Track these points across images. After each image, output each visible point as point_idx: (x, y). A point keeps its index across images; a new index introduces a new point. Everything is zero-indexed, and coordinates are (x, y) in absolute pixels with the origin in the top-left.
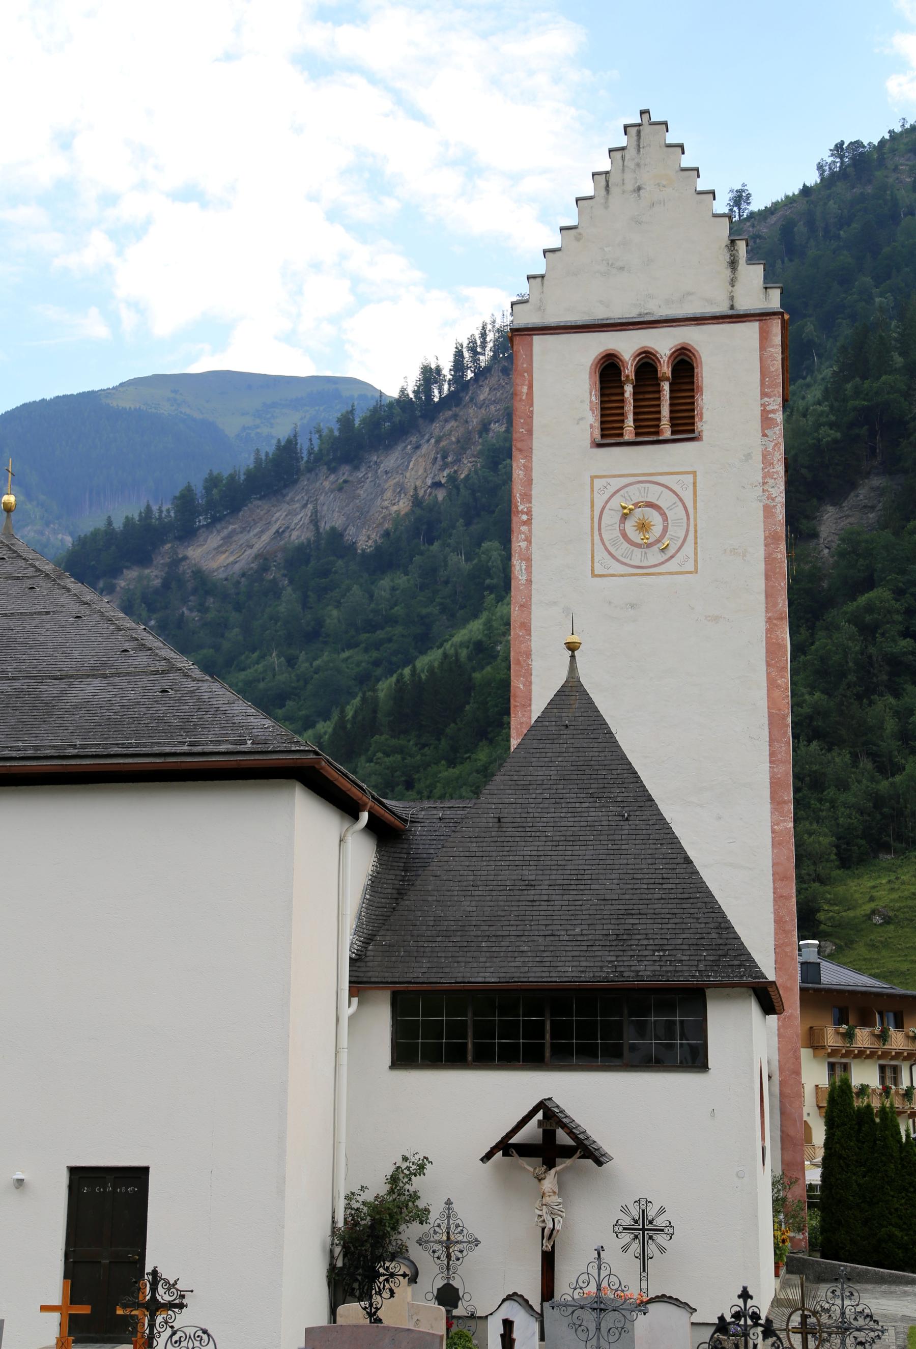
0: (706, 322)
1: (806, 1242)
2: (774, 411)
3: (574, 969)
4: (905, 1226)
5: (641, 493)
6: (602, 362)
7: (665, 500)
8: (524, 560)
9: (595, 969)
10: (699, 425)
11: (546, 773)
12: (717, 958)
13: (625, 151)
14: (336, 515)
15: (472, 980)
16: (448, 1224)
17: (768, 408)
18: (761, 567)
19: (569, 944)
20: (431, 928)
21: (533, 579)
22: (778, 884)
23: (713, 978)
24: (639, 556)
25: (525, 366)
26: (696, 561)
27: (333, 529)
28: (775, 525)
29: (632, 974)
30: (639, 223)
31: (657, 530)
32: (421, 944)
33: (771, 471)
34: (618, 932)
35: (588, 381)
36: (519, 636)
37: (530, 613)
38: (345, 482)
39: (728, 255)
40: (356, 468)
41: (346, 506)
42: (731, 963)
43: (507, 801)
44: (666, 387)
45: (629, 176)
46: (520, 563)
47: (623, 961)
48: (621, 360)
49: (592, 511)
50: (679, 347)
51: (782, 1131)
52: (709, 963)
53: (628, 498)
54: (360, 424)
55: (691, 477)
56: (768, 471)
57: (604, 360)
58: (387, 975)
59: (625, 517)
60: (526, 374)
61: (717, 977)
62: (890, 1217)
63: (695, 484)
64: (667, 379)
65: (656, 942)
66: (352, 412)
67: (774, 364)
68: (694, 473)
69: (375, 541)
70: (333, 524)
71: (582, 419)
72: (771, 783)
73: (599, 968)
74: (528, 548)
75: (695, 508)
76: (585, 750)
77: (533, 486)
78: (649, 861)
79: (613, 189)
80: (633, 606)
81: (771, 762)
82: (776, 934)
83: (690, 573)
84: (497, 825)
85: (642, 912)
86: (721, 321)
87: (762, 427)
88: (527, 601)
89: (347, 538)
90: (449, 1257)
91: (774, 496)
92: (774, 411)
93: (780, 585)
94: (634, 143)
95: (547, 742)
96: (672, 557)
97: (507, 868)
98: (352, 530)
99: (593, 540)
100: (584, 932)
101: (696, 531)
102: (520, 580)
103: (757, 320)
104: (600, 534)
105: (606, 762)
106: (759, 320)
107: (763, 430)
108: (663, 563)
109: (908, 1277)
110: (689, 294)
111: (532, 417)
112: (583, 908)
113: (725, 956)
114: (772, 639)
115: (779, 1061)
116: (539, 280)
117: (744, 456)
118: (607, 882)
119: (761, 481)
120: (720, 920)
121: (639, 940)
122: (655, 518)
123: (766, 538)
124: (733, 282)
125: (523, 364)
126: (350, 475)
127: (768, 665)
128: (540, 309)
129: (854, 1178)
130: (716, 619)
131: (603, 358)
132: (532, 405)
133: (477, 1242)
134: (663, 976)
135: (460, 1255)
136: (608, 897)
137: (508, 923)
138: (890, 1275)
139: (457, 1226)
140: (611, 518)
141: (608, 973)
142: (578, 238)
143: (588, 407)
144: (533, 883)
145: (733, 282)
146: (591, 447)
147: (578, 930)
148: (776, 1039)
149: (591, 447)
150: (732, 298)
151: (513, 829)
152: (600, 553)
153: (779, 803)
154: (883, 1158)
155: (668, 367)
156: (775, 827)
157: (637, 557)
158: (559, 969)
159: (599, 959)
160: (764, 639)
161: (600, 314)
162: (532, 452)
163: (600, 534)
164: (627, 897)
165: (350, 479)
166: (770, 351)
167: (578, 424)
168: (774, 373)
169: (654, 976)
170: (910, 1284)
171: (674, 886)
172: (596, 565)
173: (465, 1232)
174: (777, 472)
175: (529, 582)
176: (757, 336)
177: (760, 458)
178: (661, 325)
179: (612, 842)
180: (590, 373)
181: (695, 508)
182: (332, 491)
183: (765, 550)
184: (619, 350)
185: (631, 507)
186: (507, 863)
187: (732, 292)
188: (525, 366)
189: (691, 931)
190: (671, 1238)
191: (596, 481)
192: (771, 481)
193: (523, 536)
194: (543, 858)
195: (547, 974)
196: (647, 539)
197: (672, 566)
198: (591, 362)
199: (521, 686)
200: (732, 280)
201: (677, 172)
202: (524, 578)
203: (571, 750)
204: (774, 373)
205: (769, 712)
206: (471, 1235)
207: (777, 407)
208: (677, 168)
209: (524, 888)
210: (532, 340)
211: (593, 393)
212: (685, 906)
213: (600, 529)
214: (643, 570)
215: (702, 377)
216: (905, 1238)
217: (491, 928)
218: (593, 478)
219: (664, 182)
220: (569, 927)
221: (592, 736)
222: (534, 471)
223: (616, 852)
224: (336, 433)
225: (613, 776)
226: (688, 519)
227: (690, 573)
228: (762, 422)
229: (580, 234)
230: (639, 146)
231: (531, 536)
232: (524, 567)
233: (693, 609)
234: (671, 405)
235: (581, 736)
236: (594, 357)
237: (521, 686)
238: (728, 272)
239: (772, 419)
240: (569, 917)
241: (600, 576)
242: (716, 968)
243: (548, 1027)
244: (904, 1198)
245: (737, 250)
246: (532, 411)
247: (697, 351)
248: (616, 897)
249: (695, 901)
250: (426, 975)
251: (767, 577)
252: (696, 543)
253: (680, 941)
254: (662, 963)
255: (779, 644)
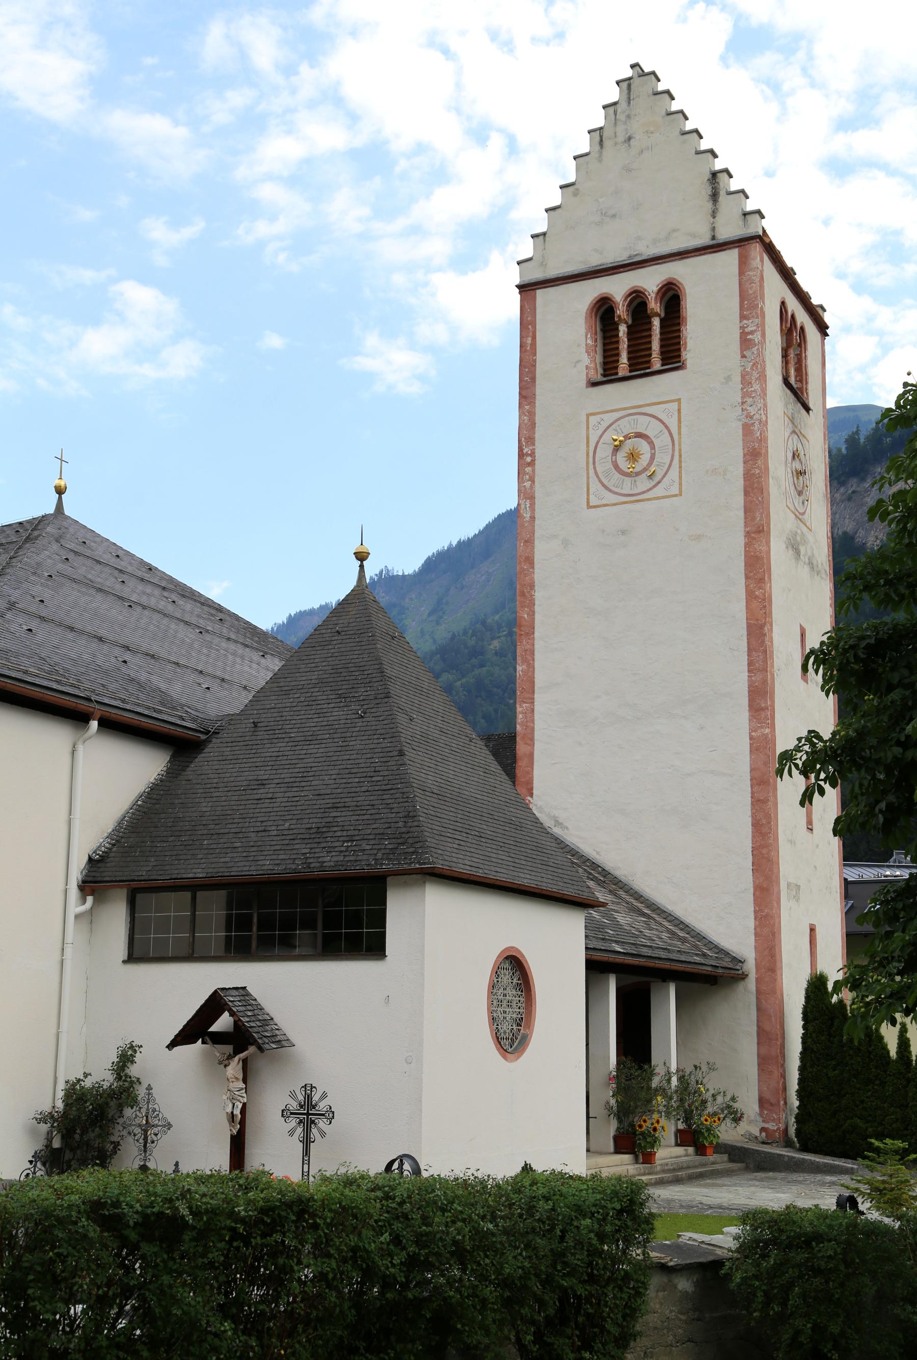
0: (689, 255)
1: (779, 1133)
2: (752, 333)
3: (271, 862)
4: (870, 1118)
5: (630, 425)
6: (597, 306)
7: (652, 429)
8: (529, 499)
9: (289, 862)
10: (684, 354)
11: (309, 678)
12: (396, 845)
13: (618, 105)
14: (847, 521)
15: (184, 876)
16: (148, 1109)
17: (747, 330)
18: (741, 483)
19: (275, 838)
20: (169, 829)
21: (536, 516)
22: (756, 788)
23: (386, 866)
24: (629, 485)
25: (529, 319)
26: (680, 484)
27: (845, 533)
28: (753, 442)
29: (318, 865)
30: (629, 170)
31: (621, 458)
32: (155, 844)
33: (750, 390)
34: (319, 825)
35: (584, 325)
36: (524, 570)
37: (533, 547)
38: (854, 492)
39: (710, 187)
40: (863, 480)
41: (856, 513)
42: (407, 850)
43: (268, 707)
44: (656, 322)
45: (620, 128)
46: (525, 502)
47: (315, 853)
48: (613, 302)
49: (588, 446)
50: (665, 283)
51: (758, 1027)
52: (388, 851)
53: (620, 431)
54: (864, 442)
55: (676, 405)
56: (747, 391)
57: (599, 304)
58: (118, 874)
59: (617, 449)
60: (530, 327)
61: (389, 865)
62: (856, 1109)
63: (679, 411)
64: (658, 315)
65: (349, 833)
66: (857, 433)
67: (751, 288)
68: (679, 400)
69: (882, 541)
70: (845, 529)
71: (578, 362)
72: (749, 692)
73: (292, 860)
74: (532, 487)
75: (680, 433)
76: (348, 653)
77: (537, 429)
78: (368, 756)
79: (607, 143)
80: (623, 532)
81: (749, 671)
82: (753, 837)
83: (675, 496)
84: (253, 730)
85: (347, 804)
86: (703, 252)
87: (741, 348)
88: (530, 536)
89: (858, 540)
90: (146, 1139)
91: (752, 414)
92: (752, 333)
93: (758, 499)
94: (625, 96)
95: (319, 648)
96: (659, 482)
97: (247, 769)
98: (861, 533)
99: (588, 474)
100: (292, 827)
101: (680, 456)
102: (525, 518)
103: (736, 247)
104: (595, 468)
105: (362, 664)
106: (738, 247)
107: (742, 352)
108: (651, 489)
109: (843, 1166)
110: (674, 230)
111: (535, 366)
112: (299, 803)
113: (403, 844)
114: (750, 552)
115: (756, 959)
116: (541, 237)
117: (724, 378)
118: (326, 778)
119: (740, 401)
120: (411, 809)
121: (335, 831)
122: (644, 447)
123: (745, 455)
124: (714, 214)
125: (527, 317)
126: (858, 486)
127: (747, 577)
128: (543, 264)
129: (825, 1071)
130: (698, 538)
131: (598, 302)
132: (535, 354)
133: (169, 1126)
134: (343, 866)
135: (155, 1138)
136: (322, 792)
137: (231, 821)
138: (826, 1165)
139: (154, 1110)
140: (604, 452)
141: (298, 865)
142: (575, 194)
143: (584, 350)
144: (265, 782)
145: (714, 214)
146: (587, 387)
147: (287, 825)
148: (753, 937)
149: (587, 387)
150: (713, 229)
151: (265, 733)
152: (595, 486)
153: (757, 711)
154: (851, 1052)
155: (656, 303)
156: (753, 734)
157: (627, 486)
158: (259, 863)
159: (295, 852)
160: (743, 553)
161: (595, 261)
162: (535, 398)
163: (595, 468)
164: (339, 791)
165: (858, 489)
166: (749, 275)
167: (575, 366)
168: (753, 296)
169: (336, 866)
170: (843, 1174)
171: (381, 778)
172: (591, 497)
173: (161, 1116)
174: (755, 391)
175: (533, 518)
176: (736, 262)
177: (739, 378)
178: (648, 264)
179: (343, 739)
180: (586, 318)
181: (680, 433)
182: (843, 501)
183: (744, 467)
184: (612, 293)
185: (621, 438)
186: (250, 765)
187: (713, 223)
188: (529, 319)
189: (382, 821)
190: (330, 1123)
191: (591, 418)
192: (749, 400)
193: (527, 477)
194: (280, 758)
195: (247, 868)
196: (634, 468)
197: (659, 491)
198: (587, 308)
199: (526, 616)
200: (713, 212)
201: (663, 117)
202: (528, 515)
203: (336, 654)
204: (753, 296)
205: (747, 623)
206: (165, 1119)
207: (755, 328)
208: (664, 113)
209: (256, 787)
210: (535, 294)
211: (589, 336)
212: (385, 797)
213: (594, 463)
214: (634, 498)
215: (686, 308)
216: (870, 1130)
217: (217, 827)
218: (588, 415)
219: (652, 129)
220: (281, 822)
221: (358, 640)
222: (537, 415)
223: (344, 748)
224: (844, 451)
225: (363, 677)
226: (673, 445)
227: (675, 496)
228: (741, 344)
229: (577, 189)
230: (629, 98)
231: (534, 476)
232: (528, 505)
233: (677, 530)
234: (661, 340)
235: (348, 641)
236: (589, 302)
237: (526, 616)
238: (709, 205)
239: (750, 340)
240: (283, 813)
241: (595, 507)
242: (391, 856)
243: (255, 920)
244: (870, 1090)
245: (718, 183)
246: (536, 359)
247: (682, 284)
248: (329, 791)
249: (395, 791)
250: (150, 873)
251: (746, 493)
252: (680, 467)
253: (369, 831)
254: (347, 854)
255: (757, 556)
